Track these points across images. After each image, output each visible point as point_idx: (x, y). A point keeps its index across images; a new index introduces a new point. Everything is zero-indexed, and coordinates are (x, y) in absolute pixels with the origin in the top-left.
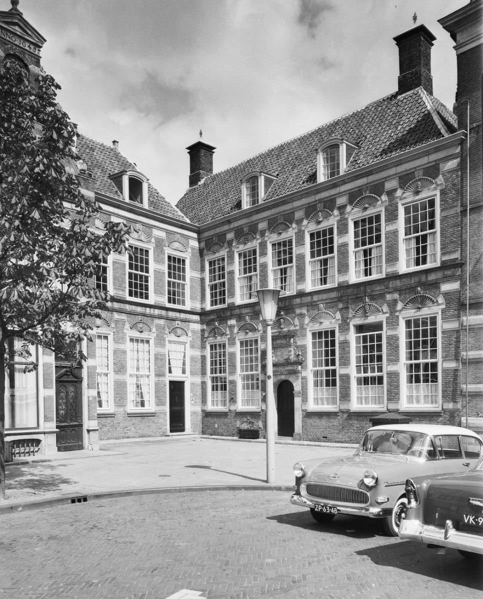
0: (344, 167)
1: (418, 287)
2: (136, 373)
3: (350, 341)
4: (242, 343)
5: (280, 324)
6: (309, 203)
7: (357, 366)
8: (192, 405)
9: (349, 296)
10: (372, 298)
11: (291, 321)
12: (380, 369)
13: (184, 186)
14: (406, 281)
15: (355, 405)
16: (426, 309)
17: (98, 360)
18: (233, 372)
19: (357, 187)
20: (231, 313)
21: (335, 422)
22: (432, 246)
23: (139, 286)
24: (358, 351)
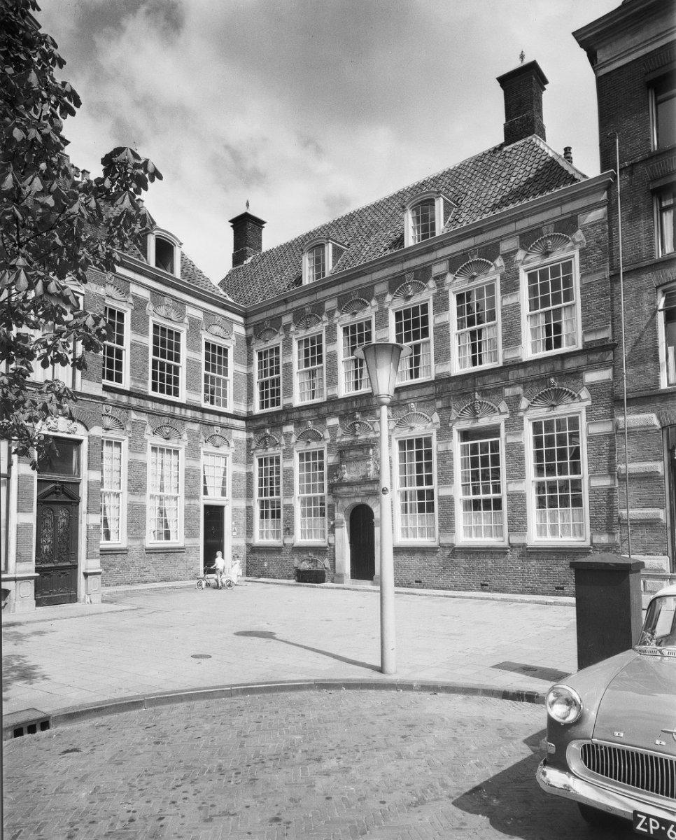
0: (440, 228)
1: (551, 379)
2: (160, 494)
3: (454, 451)
4: (301, 456)
5: (355, 430)
6: (395, 274)
7: (462, 485)
8: (234, 537)
9: (450, 392)
10: (484, 393)
11: (370, 427)
12: (497, 489)
13: (227, 265)
14: (533, 371)
15: (462, 538)
16: (564, 406)
17: (105, 475)
18: (289, 494)
19: (460, 251)
20: (287, 417)
21: (433, 561)
22: (569, 323)
23: (166, 378)
24: (464, 465)
